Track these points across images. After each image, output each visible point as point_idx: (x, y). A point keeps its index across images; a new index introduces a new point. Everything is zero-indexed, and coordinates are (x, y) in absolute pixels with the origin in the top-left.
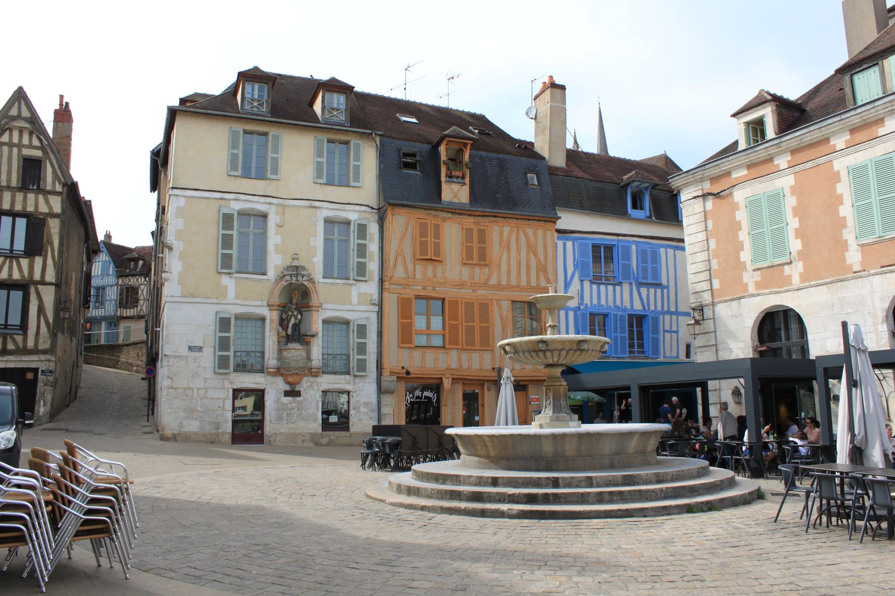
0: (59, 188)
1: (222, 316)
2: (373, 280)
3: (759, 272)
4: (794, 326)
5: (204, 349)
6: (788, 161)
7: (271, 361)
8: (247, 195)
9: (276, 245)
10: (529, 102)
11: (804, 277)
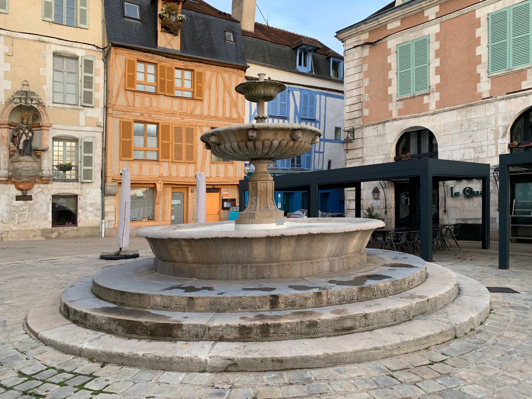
2: (98, 107)
3: (402, 102)
4: (426, 143)
6: (437, 13)
11: (439, 104)
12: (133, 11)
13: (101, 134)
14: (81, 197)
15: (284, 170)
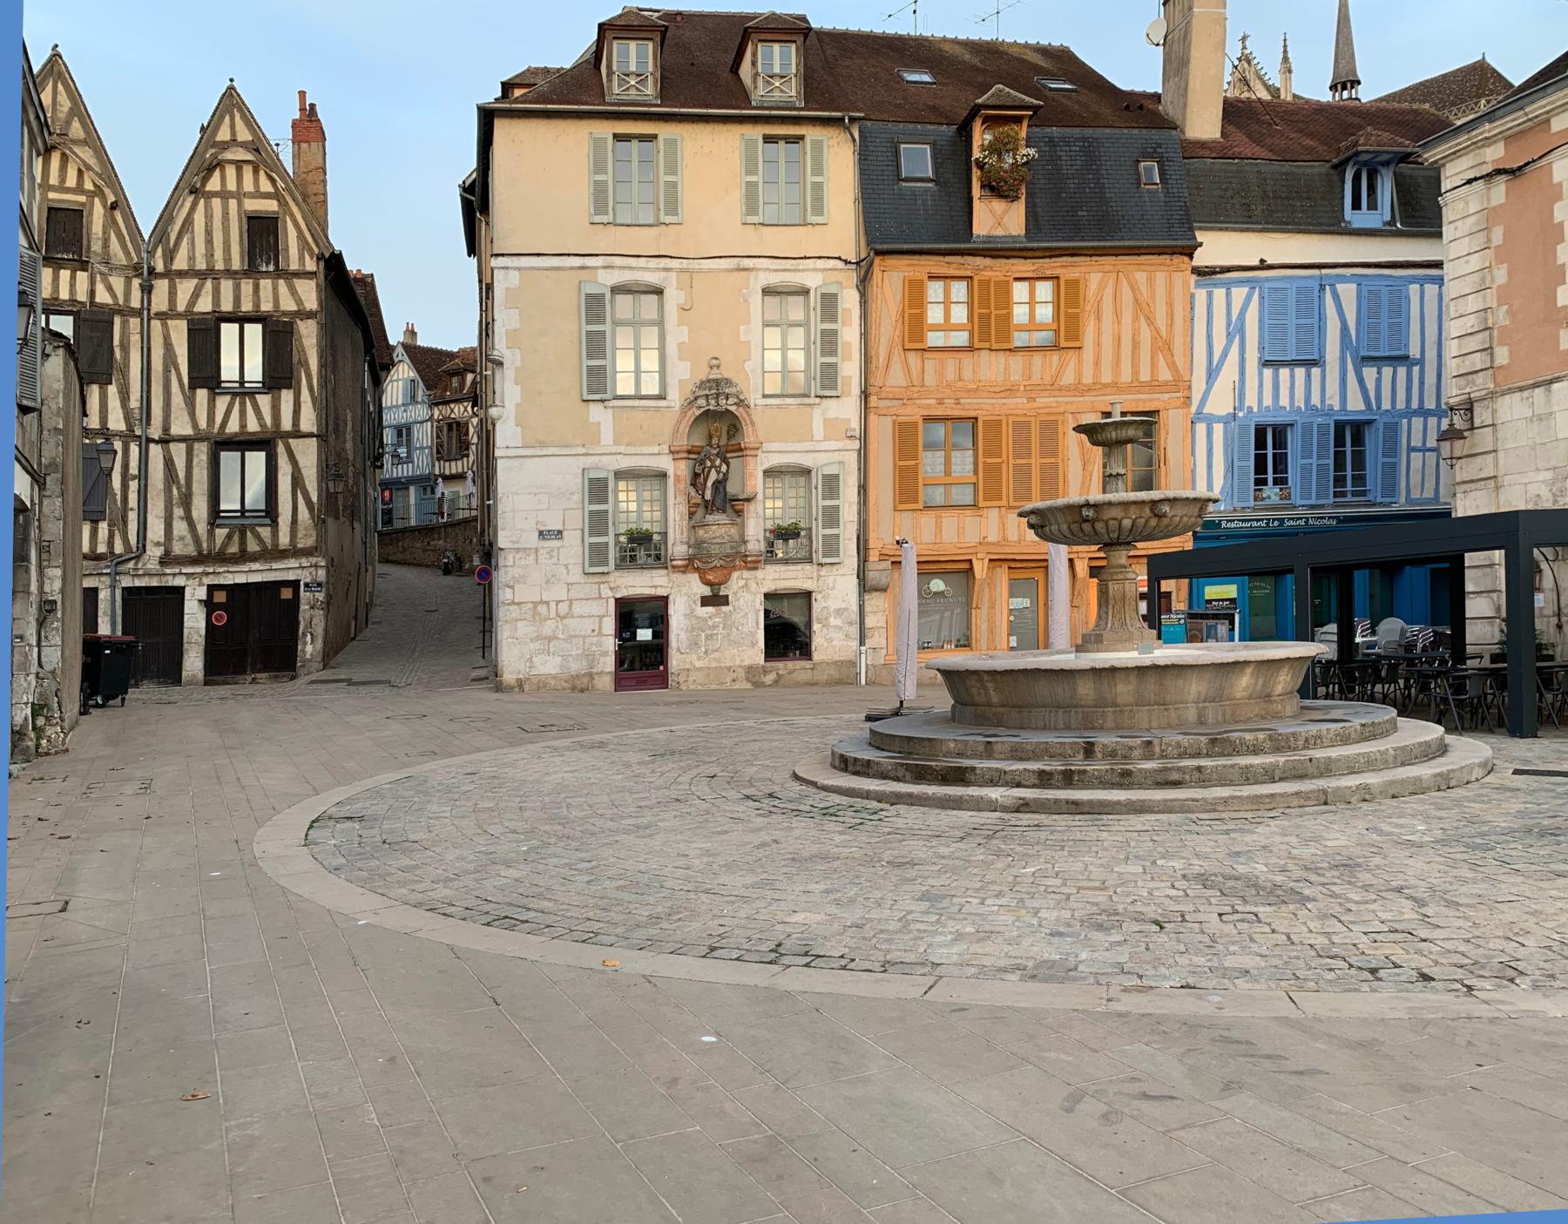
0: (311, 265)
1: (593, 475)
7: (678, 548)
12: (918, 160)
13: (855, 455)
15: (1312, 507)
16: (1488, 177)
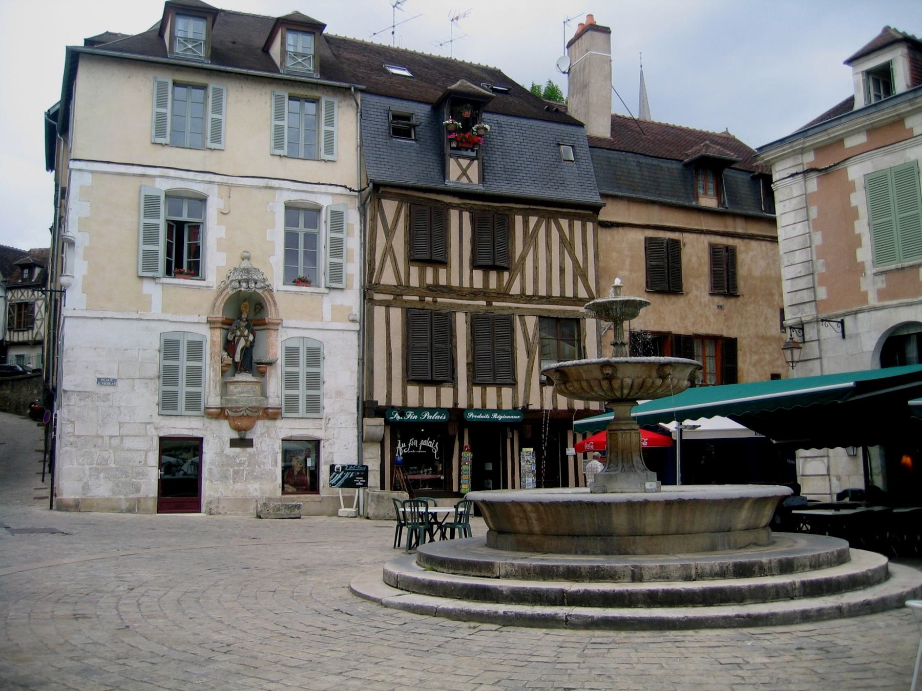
3: (883, 277)
5: (120, 383)
8: (178, 169)
9: (219, 240)
10: (559, 49)
14: (326, 444)
16: (806, 172)
